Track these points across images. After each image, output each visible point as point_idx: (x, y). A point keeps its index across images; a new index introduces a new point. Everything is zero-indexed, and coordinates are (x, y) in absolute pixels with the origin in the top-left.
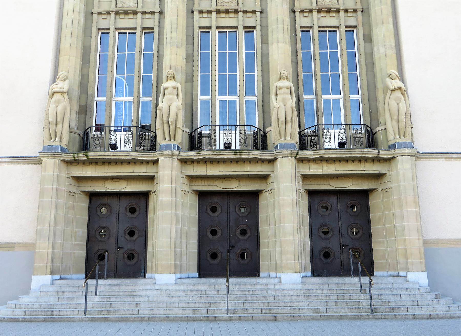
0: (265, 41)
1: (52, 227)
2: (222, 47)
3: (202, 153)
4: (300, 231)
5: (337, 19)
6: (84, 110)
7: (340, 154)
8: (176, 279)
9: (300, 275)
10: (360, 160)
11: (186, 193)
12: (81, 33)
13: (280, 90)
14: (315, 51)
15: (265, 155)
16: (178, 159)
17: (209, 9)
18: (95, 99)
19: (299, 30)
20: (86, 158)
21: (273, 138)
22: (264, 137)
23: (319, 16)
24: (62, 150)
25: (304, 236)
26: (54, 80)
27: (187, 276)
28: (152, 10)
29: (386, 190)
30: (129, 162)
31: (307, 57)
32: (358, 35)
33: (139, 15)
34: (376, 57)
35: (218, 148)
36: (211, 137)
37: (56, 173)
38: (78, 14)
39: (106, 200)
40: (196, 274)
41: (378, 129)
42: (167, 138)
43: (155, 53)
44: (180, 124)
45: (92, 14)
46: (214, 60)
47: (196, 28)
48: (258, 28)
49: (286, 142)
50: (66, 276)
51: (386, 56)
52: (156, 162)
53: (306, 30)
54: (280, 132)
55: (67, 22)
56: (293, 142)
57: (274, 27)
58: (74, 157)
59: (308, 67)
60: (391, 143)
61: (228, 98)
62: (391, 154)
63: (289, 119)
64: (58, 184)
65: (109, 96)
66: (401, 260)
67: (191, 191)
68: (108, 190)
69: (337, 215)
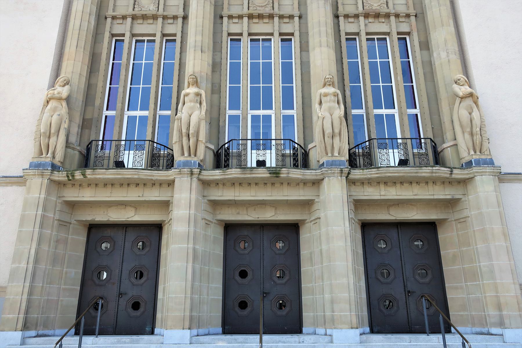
0: (304, 48)
1: (31, 266)
2: (254, 56)
3: (229, 171)
4: (355, 272)
5: (387, 25)
6: (86, 124)
7: (404, 172)
8: (191, 337)
9: (358, 332)
10: (426, 181)
11: (208, 223)
12: (90, 37)
13: (325, 98)
14: (363, 61)
15: (308, 174)
16: (199, 180)
17: (240, 13)
18: (104, 112)
19: (343, 37)
20: (82, 177)
21: (316, 155)
22: (306, 155)
23: (367, 22)
24: (54, 168)
25: (359, 279)
26: (52, 85)
27: (207, 333)
28: (175, 14)
29: (462, 220)
30: (138, 184)
31: (354, 67)
32: (413, 44)
33: (160, 20)
34: (437, 63)
35: (249, 165)
36: (241, 157)
37: (43, 196)
38: (88, 15)
39: (109, 232)
40: (220, 330)
41: (445, 146)
42: (186, 154)
43: (177, 62)
44: (202, 137)
45: (106, 18)
46: (245, 68)
47: (225, 34)
48: (297, 34)
49: (334, 159)
50: (46, 332)
51: (449, 61)
52: (171, 184)
53: (352, 38)
54: (326, 147)
55: (75, 23)
56: (343, 159)
57: (316, 30)
58: (68, 176)
59: (355, 78)
60: (464, 161)
61: (261, 112)
62: (468, 174)
63: (337, 131)
64: (45, 209)
65: (120, 108)
66: (492, 312)
67: (215, 221)
68: (111, 219)
69: (399, 252)
